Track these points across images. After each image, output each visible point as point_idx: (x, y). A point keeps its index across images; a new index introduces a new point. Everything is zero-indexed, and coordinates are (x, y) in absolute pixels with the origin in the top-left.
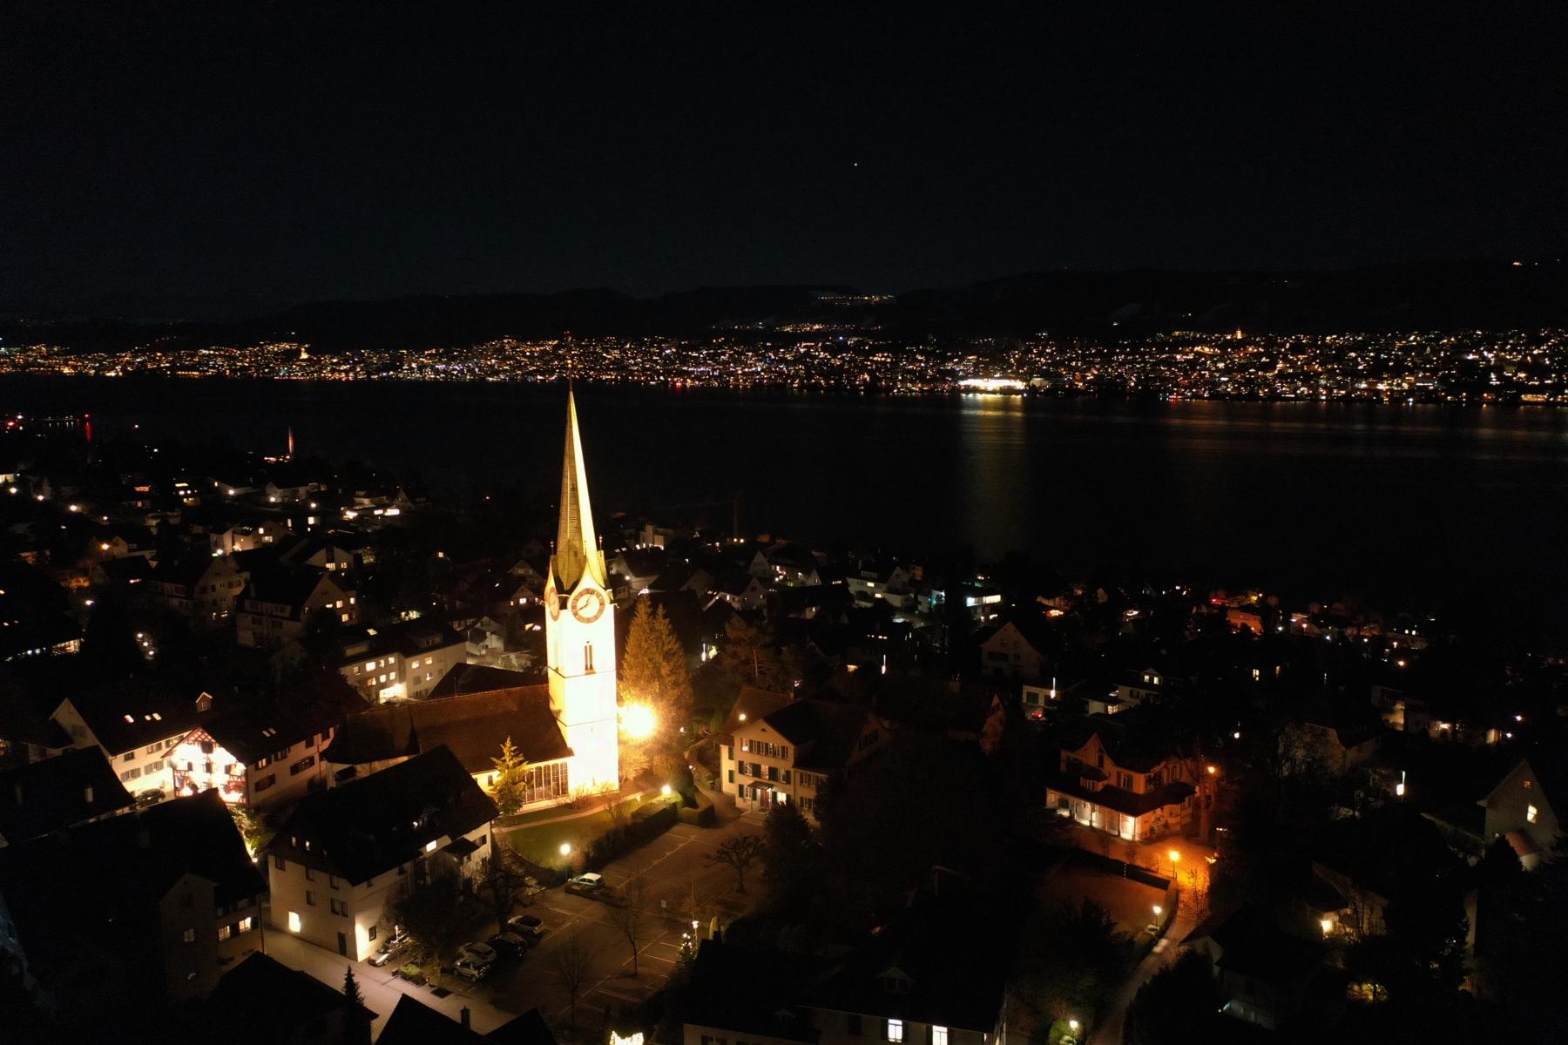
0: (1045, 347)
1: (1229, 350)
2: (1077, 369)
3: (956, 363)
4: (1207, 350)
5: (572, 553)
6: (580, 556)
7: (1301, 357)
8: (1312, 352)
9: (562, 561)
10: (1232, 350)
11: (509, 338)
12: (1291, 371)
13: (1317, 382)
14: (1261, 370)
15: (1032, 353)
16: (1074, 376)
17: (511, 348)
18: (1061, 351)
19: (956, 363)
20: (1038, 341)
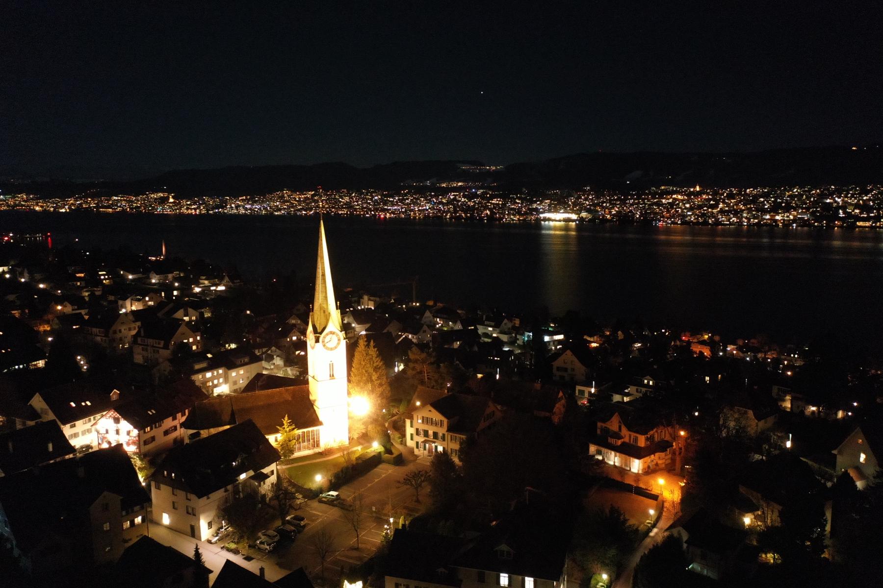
0: (588, 195)
1: (692, 197)
2: (606, 207)
3: (538, 204)
5: (322, 311)
6: (327, 313)
7: (733, 201)
8: (739, 198)
9: (316, 316)
10: (694, 197)
13: (742, 215)
14: (710, 208)
15: (581, 199)
16: (605, 211)
18: (598, 198)
19: (538, 204)
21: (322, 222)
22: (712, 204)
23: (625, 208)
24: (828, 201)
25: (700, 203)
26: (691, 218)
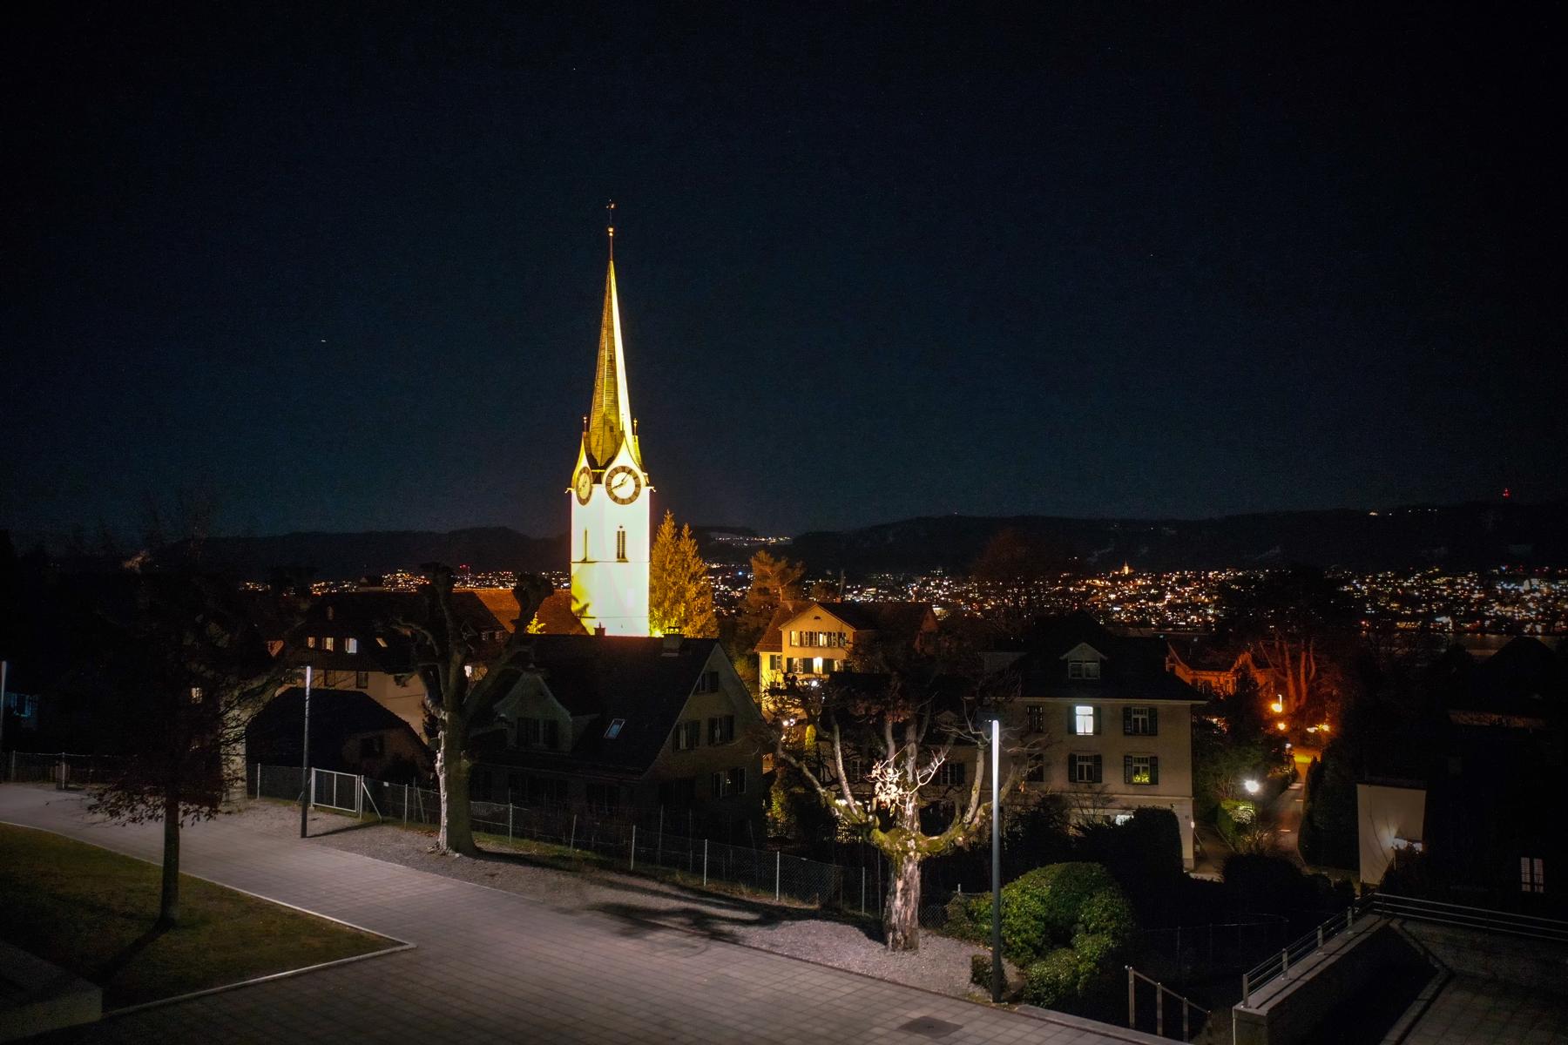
0: (942, 580)
1: (1119, 583)
2: (974, 599)
3: (855, 595)
4: (1098, 582)
5: (607, 428)
6: (616, 432)
7: (1188, 589)
8: (1197, 584)
9: (596, 434)
10: (1122, 583)
11: (403, 572)
12: (1180, 601)
15: (930, 585)
19: (855, 595)
20: (934, 577)
21: (612, 262)
22: (1153, 594)
23: (1006, 601)
24: (1346, 588)
25: (1133, 593)
26: (1121, 616)
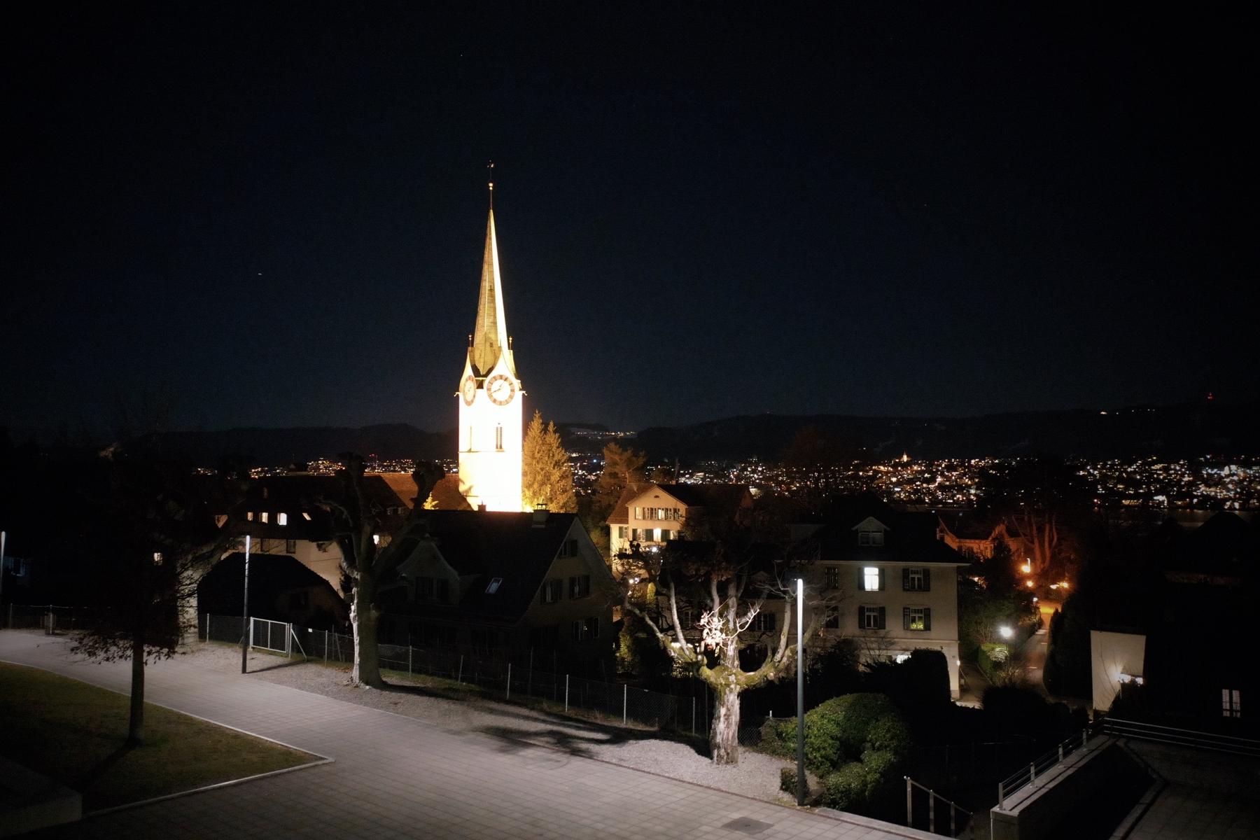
1: (899, 468)
2: (783, 482)
4: (882, 468)
5: (488, 344)
7: (954, 473)
8: (962, 470)
9: (478, 353)
10: (902, 468)
12: (948, 483)
14: (925, 483)
15: (747, 470)
16: (781, 487)
17: (325, 467)
19: (687, 478)
21: (491, 211)
23: (808, 483)
25: (910, 477)
